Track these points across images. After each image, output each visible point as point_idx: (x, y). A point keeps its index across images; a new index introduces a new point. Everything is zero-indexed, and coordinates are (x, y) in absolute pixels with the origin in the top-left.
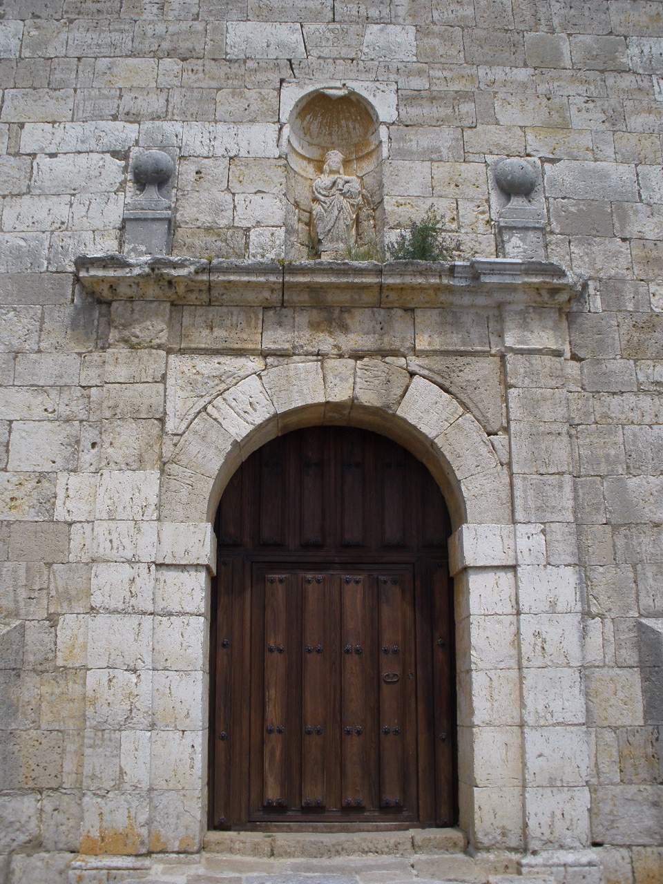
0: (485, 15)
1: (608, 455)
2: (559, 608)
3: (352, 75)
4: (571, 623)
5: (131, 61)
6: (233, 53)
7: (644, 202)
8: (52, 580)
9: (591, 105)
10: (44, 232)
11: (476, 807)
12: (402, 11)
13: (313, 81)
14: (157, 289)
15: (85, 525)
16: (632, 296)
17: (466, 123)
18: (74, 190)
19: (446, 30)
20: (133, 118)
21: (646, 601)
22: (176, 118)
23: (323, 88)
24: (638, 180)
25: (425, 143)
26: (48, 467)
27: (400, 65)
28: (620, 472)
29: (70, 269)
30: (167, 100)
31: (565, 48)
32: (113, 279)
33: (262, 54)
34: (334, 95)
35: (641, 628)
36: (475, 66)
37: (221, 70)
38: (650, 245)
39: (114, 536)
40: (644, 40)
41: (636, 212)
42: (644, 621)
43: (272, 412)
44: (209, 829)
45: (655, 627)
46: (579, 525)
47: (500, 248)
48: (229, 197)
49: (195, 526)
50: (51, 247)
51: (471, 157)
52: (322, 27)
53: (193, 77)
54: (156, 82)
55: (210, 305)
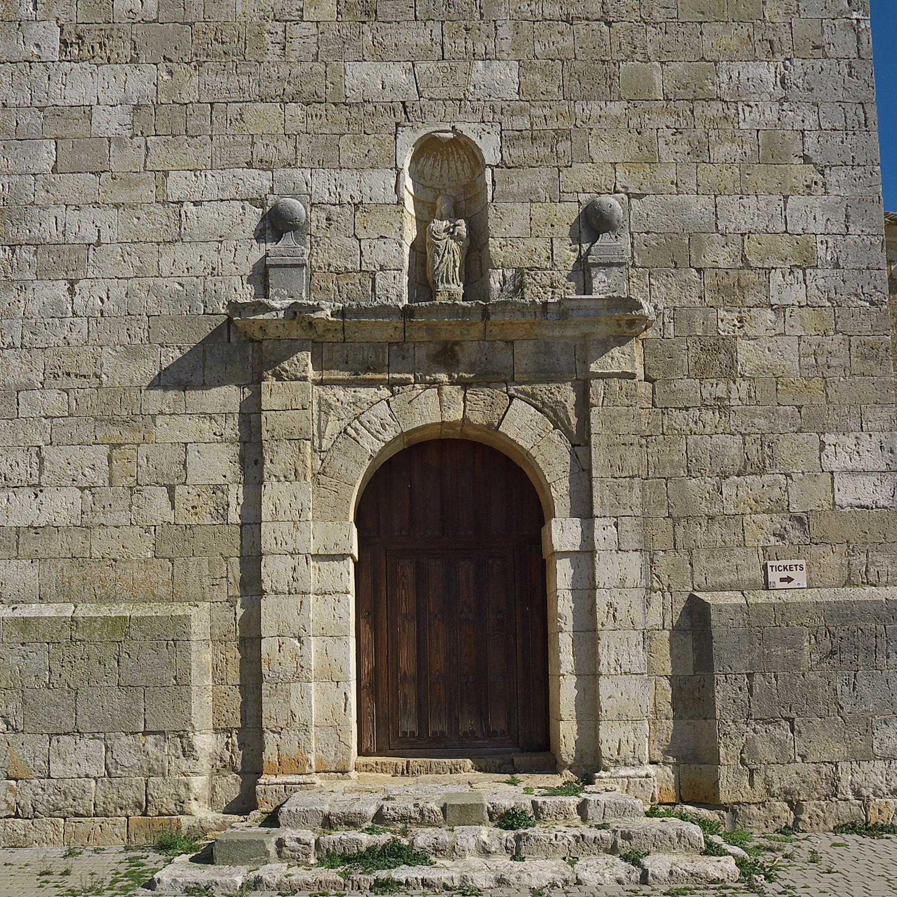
0: (584, 46)
1: (672, 461)
2: (628, 584)
3: (460, 118)
4: (638, 595)
5: (260, 106)
6: (353, 97)
7: (720, 232)
8: (230, 570)
9: (679, 136)
10: (197, 277)
11: (561, 735)
12: (505, 45)
13: (425, 125)
14: (300, 330)
15: (253, 526)
16: (702, 322)
17: (562, 163)
18: (220, 237)
19: (547, 64)
20: (266, 166)
21: (699, 579)
22: (304, 165)
23: (434, 132)
24: (716, 211)
25: (525, 185)
26: (220, 480)
27: (504, 104)
28: (682, 475)
29: (223, 311)
30: (296, 147)
31: (658, 77)
32: (262, 321)
33: (378, 97)
34: (443, 138)
35: (692, 597)
36: (573, 102)
37: (343, 115)
38: (722, 273)
39: (278, 534)
40: (732, 66)
41: (712, 243)
42: (696, 594)
43: (399, 431)
44: (359, 755)
45: (706, 599)
46: (646, 520)
47: (586, 288)
48: (355, 243)
49: (341, 524)
50: (205, 290)
51: (566, 197)
52: (432, 65)
53: (318, 122)
54: (284, 127)
55: (344, 342)
